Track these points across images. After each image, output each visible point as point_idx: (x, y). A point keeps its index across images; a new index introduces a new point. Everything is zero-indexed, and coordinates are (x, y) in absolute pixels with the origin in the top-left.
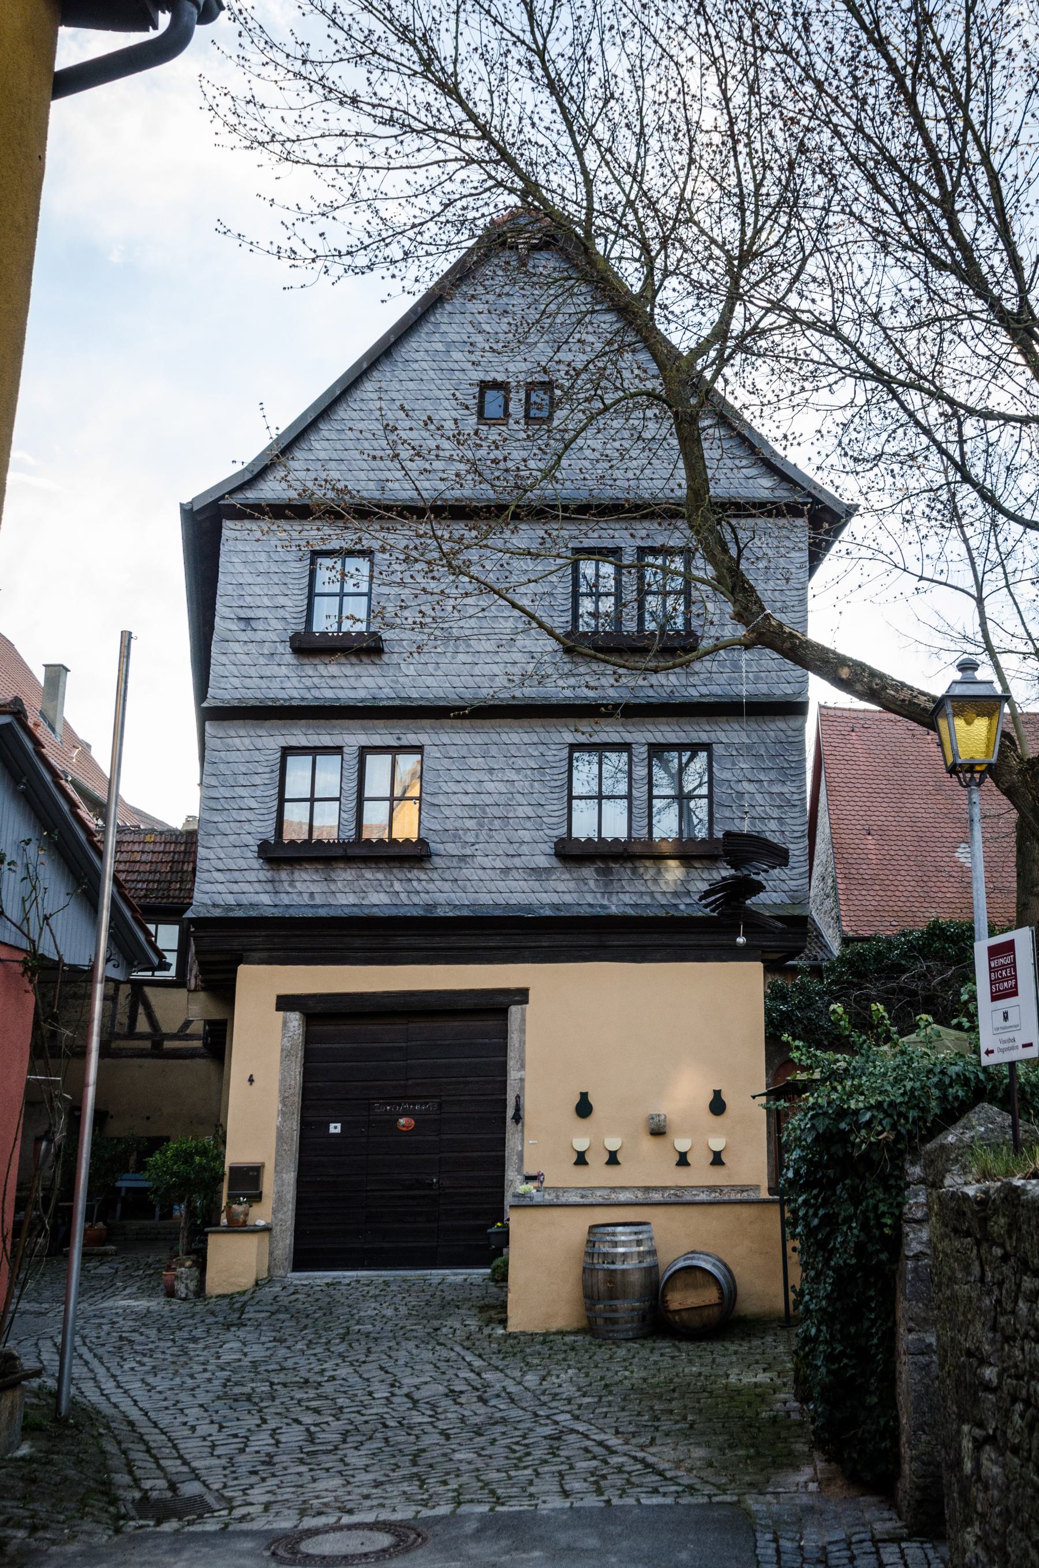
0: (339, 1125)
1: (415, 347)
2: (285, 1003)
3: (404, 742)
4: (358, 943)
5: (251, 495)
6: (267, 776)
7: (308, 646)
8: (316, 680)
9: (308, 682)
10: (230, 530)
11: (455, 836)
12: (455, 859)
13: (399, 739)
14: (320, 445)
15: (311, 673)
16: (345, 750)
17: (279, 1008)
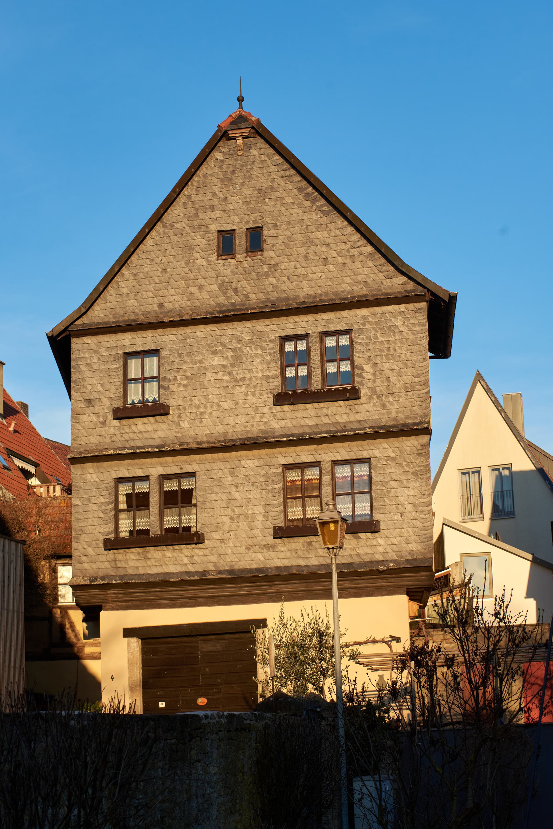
0: (164, 703)
1: (176, 211)
2: (128, 633)
3: (185, 471)
4: (166, 595)
5: (85, 320)
6: (107, 497)
7: (124, 413)
8: (131, 435)
9: (126, 437)
10: (77, 344)
11: (217, 527)
12: (217, 542)
13: (181, 469)
14: (124, 282)
15: (128, 431)
16: (151, 478)
17: (125, 636)
